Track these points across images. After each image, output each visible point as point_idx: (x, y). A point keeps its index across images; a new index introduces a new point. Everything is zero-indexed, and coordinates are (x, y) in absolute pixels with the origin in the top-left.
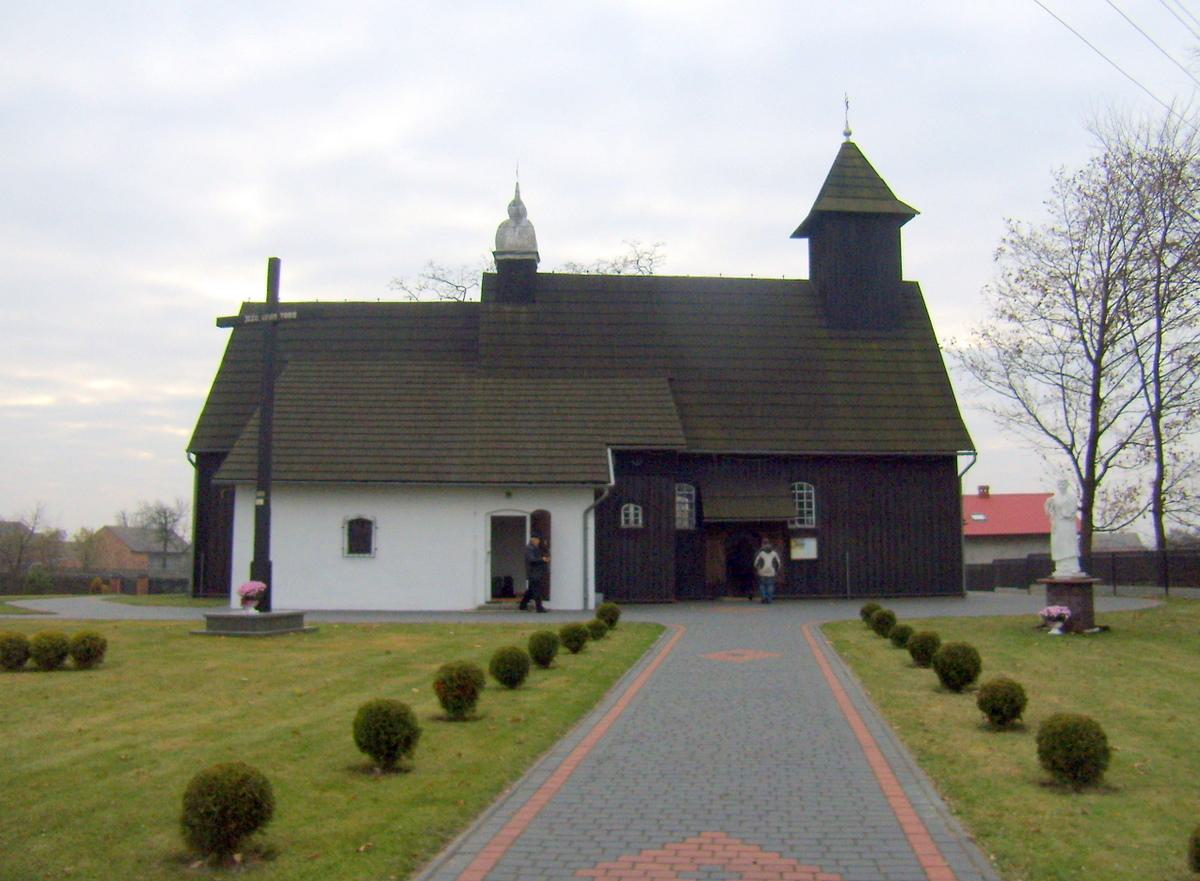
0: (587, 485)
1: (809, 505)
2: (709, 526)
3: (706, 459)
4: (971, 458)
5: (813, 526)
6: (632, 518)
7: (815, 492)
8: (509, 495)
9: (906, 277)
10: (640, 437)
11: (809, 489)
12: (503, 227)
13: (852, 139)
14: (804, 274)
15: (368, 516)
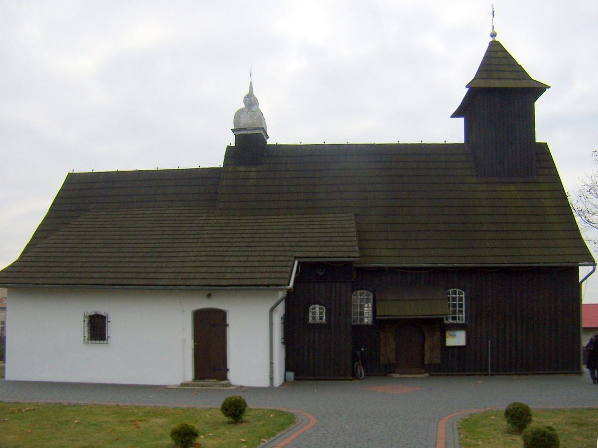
0: (271, 287)
1: (461, 306)
2: (381, 321)
3: (380, 271)
4: (591, 268)
5: (464, 322)
6: (318, 315)
7: (466, 296)
8: (209, 296)
9: (538, 139)
10: (318, 252)
11: (460, 293)
12: (240, 112)
13: (497, 39)
14: (461, 140)
15: (102, 312)
